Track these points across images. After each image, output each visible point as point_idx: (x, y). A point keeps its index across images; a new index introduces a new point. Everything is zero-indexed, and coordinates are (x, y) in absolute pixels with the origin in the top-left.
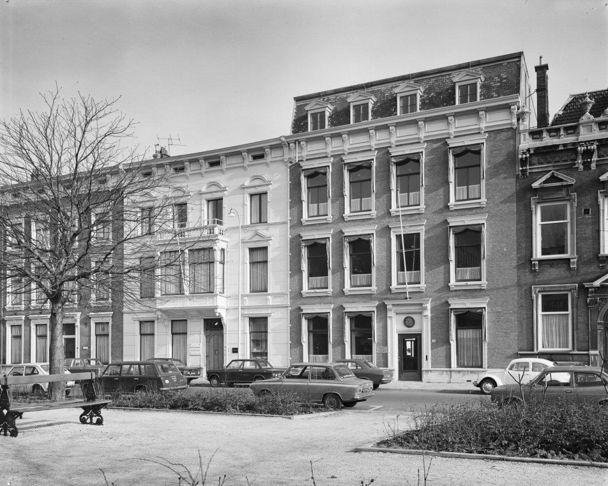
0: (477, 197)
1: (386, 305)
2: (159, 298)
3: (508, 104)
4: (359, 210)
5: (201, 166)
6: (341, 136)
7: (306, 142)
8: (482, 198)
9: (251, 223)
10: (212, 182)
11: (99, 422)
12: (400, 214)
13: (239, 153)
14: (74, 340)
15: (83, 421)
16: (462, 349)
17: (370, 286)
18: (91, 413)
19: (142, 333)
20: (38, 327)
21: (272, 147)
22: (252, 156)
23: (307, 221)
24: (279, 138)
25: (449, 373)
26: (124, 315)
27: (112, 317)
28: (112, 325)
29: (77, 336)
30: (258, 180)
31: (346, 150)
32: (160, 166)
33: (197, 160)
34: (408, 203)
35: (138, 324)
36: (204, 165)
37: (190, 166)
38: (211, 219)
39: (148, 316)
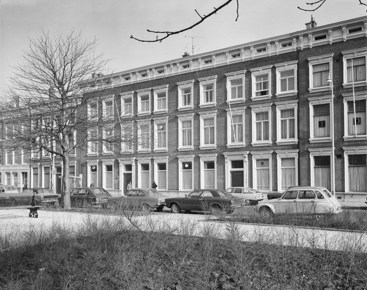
1: (224, 156)
5: (120, 80)
11: (37, 217)
14: (131, 174)
15: (30, 216)
16: (292, 175)
18: (34, 212)
21: (114, 78)
23: (312, 90)
31: (311, 45)
33: (248, 48)
34: (321, 85)
37: (304, 40)
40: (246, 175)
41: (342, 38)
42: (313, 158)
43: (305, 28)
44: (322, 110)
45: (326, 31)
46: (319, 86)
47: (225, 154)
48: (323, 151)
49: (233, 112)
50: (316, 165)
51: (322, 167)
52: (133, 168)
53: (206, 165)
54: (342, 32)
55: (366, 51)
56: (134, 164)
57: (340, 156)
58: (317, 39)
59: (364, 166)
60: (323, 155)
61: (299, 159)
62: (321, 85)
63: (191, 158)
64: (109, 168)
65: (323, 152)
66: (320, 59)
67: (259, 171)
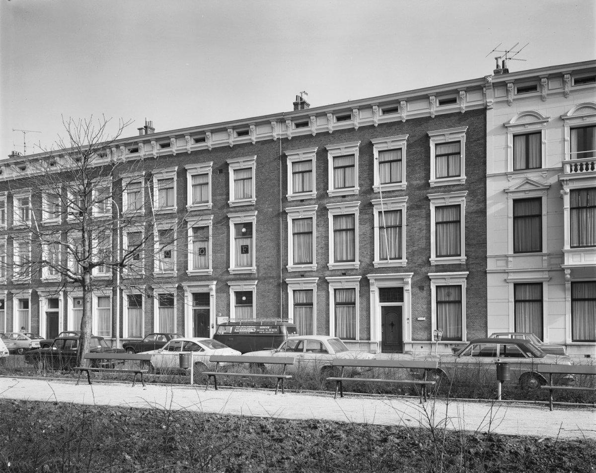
0: (457, 174)
2: (568, 252)
3: (427, 95)
4: (446, 176)
6: (326, 115)
7: (255, 126)
8: (403, 181)
9: (514, 170)
10: (584, 104)
12: (381, 190)
13: (370, 107)
14: (57, 313)
17: (460, 255)
19: (576, 297)
20: (337, 292)
21: (551, 77)
22: (194, 139)
24: (484, 78)
25: (429, 346)
26: (489, 276)
27: (467, 279)
28: (467, 289)
29: (61, 310)
30: (587, 109)
32: (145, 142)
34: (345, 185)
35: (512, 287)
36: (190, 142)
38: (575, 153)
39: (537, 277)
40: (61, 318)
41: (373, 121)
42: (126, 296)
43: (291, 108)
44: (246, 230)
45: (457, 92)
46: (241, 199)
47: (39, 291)
48: (245, 285)
49: (385, 206)
50: (237, 303)
51: (241, 306)
52: (61, 304)
53: (22, 303)
54: (430, 103)
55: (594, 116)
56: (61, 298)
57: (151, 297)
58: (442, 103)
59: (171, 308)
60: (244, 290)
61: (113, 298)
62: (345, 185)
63: (171, 289)
64: (24, 303)
65: (244, 287)
66: (447, 134)
67: (76, 312)
